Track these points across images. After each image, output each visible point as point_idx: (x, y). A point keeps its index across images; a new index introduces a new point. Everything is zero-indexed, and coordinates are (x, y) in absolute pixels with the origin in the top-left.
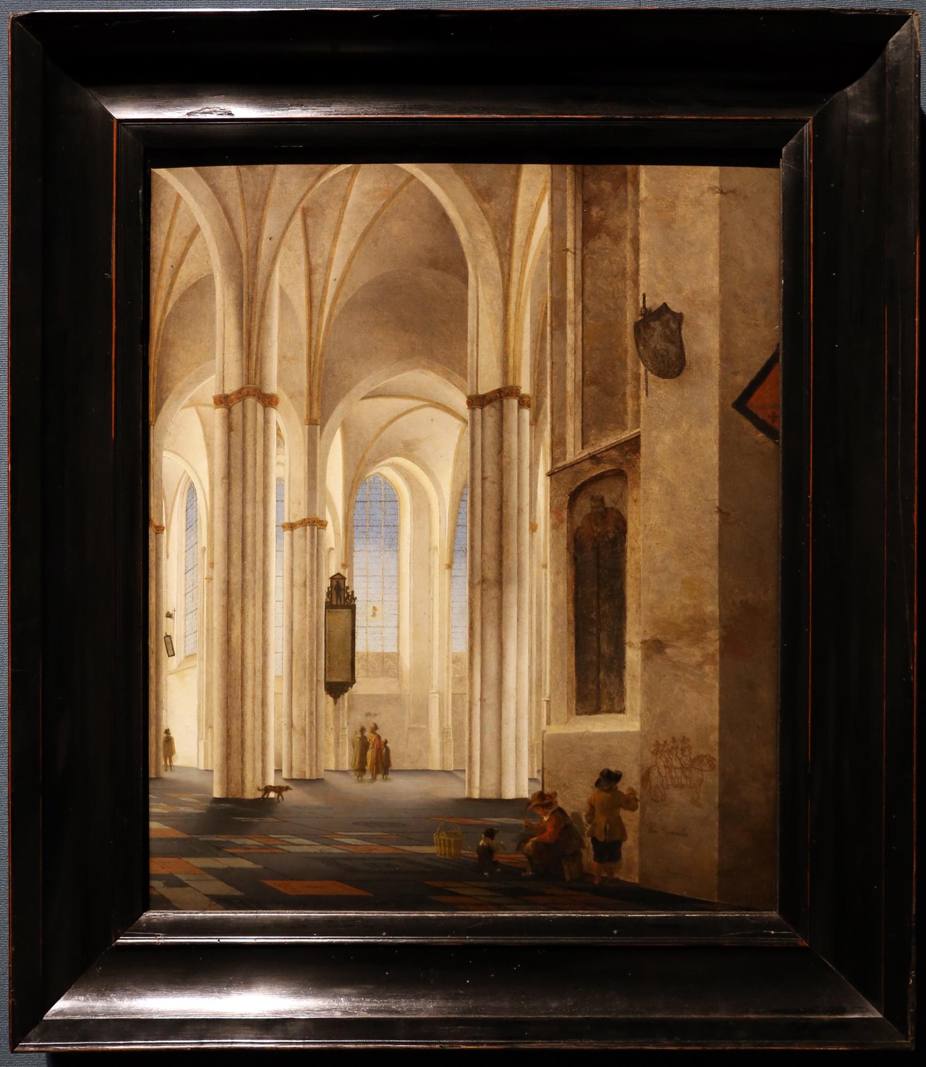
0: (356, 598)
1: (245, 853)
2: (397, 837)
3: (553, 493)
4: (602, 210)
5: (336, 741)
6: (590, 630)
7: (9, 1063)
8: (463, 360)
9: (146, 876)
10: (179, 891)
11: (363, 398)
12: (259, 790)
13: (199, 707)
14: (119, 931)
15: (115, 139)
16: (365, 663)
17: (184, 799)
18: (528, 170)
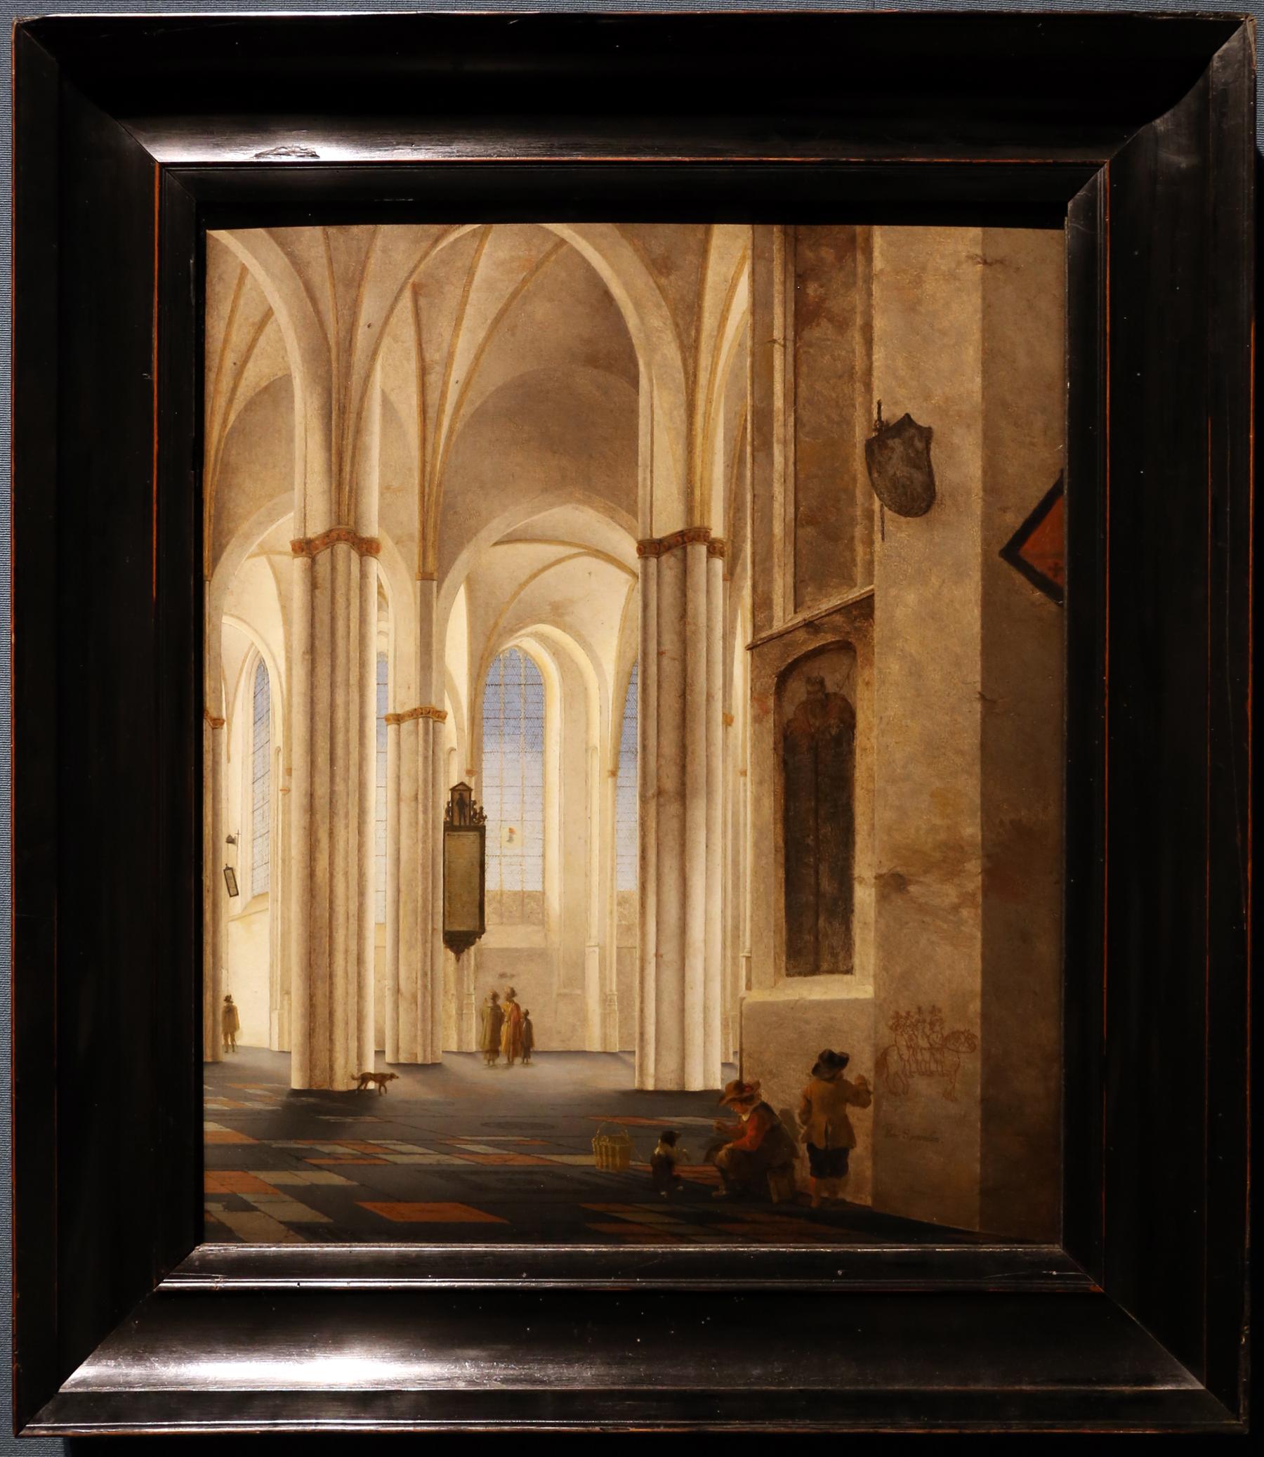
0: (486, 817)
1: (334, 1165)
2: (543, 1143)
3: (755, 673)
4: (822, 286)
5: (459, 1012)
6: (806, 861)
7: (12, 1451)
8: (631, 491)
9: (199, 1196)
10: (244, 1216)
11: (496, 544)
12: (354, 1078)
13: (272, 966)
14: (163, 1271)
15: (157, 190)
16: (499, 906)
17: (251, 1091)
18: (721, 232)
